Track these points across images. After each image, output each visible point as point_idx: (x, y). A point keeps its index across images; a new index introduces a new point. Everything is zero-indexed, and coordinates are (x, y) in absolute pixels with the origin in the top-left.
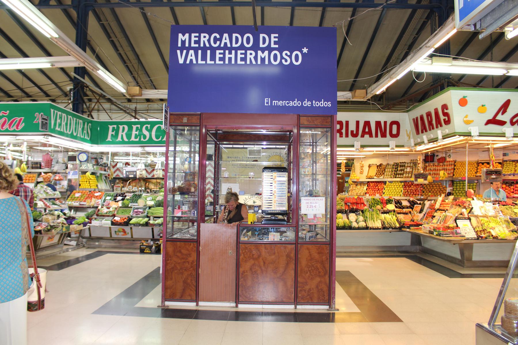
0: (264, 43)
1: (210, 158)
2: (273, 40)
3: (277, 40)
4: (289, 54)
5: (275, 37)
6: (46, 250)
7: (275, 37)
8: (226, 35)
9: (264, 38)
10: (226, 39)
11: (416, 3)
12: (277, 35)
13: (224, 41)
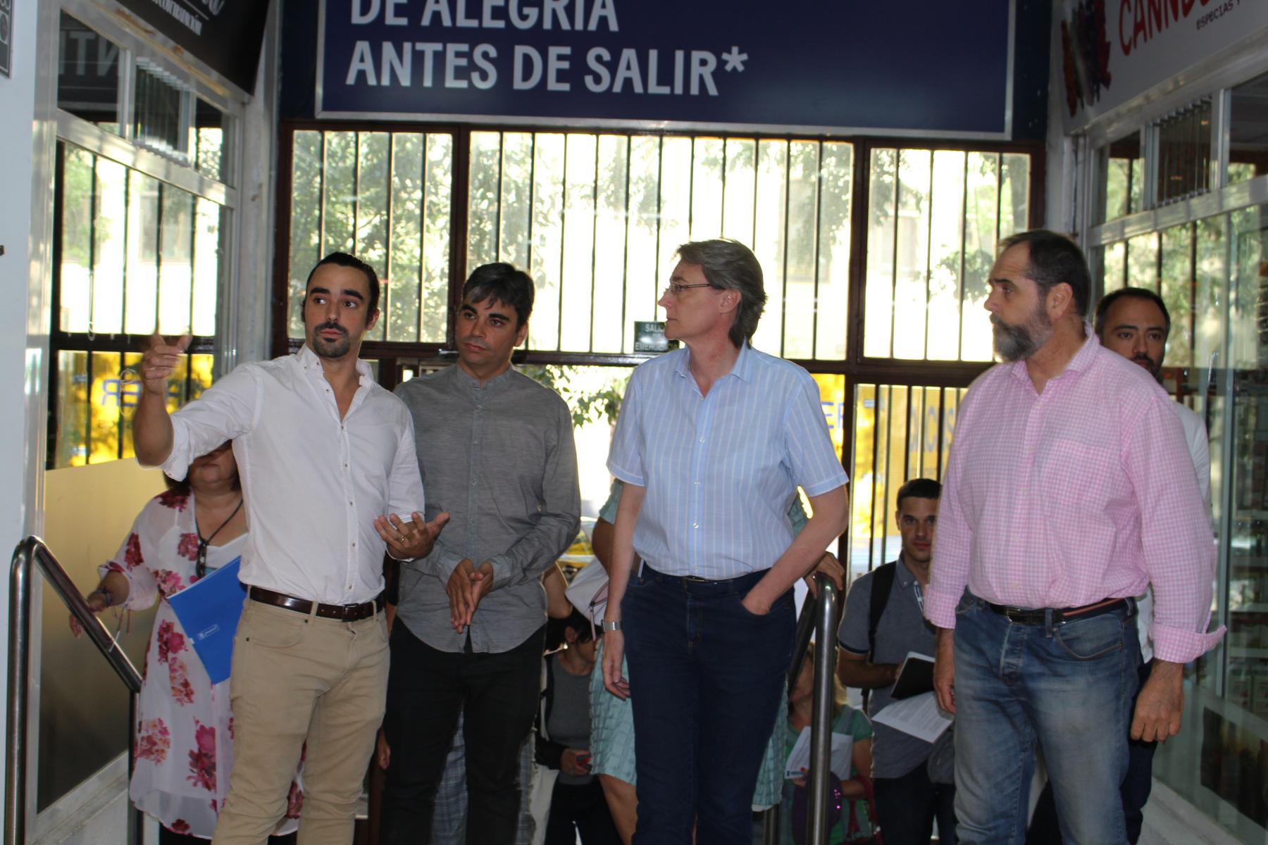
0: (527, 75)
1: (576, 71)
2: (554, 65)
3: (565, 65)
4: (607, 56)
5: (561, 58)
6: (146, 233)
7: (561, 58)
8: (629, 54)
9: (527, 60)
10: (628, 68)
11: (1030, 226)
12: (566, 51)
13: (622, 73)
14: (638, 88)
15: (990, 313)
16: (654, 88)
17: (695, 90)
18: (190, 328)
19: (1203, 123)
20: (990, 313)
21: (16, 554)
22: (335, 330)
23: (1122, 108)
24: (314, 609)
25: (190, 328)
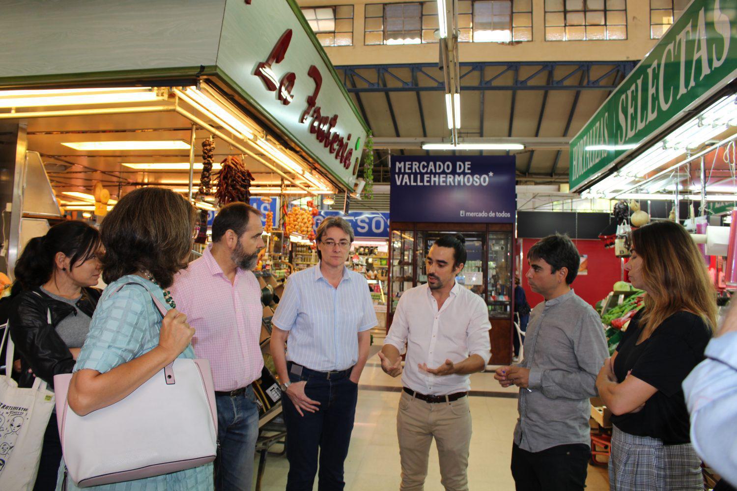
2: (467, 166)
3: (469, 166)
5: (468, 165)
7: (468, 165)
9: (440, 166)
12: (470, 163)
13: (430, 168)
14: (408, 184)
15: (516, 200)
16: (413, 184)
17: (404, 184)
18: (622, 10)
19: (4, 178)
20: (516, 200)
21: (396, 376)
22: (433, 277)
23: (130, 189)
24: (447, 398)
25: (622, 10)
